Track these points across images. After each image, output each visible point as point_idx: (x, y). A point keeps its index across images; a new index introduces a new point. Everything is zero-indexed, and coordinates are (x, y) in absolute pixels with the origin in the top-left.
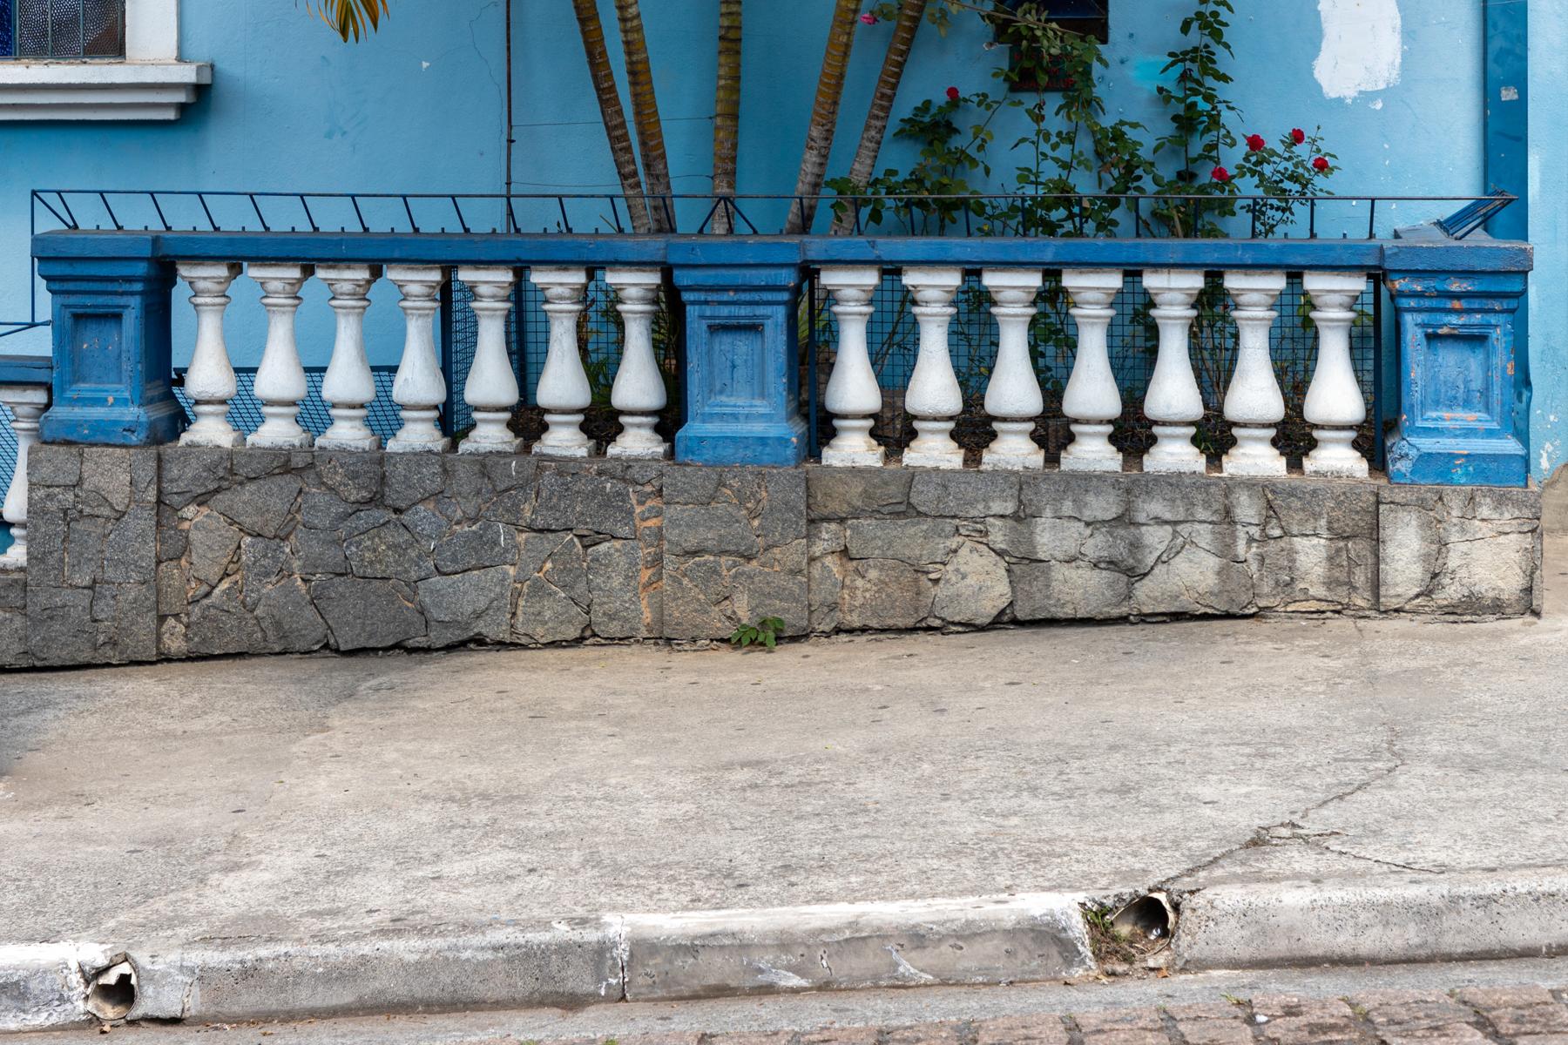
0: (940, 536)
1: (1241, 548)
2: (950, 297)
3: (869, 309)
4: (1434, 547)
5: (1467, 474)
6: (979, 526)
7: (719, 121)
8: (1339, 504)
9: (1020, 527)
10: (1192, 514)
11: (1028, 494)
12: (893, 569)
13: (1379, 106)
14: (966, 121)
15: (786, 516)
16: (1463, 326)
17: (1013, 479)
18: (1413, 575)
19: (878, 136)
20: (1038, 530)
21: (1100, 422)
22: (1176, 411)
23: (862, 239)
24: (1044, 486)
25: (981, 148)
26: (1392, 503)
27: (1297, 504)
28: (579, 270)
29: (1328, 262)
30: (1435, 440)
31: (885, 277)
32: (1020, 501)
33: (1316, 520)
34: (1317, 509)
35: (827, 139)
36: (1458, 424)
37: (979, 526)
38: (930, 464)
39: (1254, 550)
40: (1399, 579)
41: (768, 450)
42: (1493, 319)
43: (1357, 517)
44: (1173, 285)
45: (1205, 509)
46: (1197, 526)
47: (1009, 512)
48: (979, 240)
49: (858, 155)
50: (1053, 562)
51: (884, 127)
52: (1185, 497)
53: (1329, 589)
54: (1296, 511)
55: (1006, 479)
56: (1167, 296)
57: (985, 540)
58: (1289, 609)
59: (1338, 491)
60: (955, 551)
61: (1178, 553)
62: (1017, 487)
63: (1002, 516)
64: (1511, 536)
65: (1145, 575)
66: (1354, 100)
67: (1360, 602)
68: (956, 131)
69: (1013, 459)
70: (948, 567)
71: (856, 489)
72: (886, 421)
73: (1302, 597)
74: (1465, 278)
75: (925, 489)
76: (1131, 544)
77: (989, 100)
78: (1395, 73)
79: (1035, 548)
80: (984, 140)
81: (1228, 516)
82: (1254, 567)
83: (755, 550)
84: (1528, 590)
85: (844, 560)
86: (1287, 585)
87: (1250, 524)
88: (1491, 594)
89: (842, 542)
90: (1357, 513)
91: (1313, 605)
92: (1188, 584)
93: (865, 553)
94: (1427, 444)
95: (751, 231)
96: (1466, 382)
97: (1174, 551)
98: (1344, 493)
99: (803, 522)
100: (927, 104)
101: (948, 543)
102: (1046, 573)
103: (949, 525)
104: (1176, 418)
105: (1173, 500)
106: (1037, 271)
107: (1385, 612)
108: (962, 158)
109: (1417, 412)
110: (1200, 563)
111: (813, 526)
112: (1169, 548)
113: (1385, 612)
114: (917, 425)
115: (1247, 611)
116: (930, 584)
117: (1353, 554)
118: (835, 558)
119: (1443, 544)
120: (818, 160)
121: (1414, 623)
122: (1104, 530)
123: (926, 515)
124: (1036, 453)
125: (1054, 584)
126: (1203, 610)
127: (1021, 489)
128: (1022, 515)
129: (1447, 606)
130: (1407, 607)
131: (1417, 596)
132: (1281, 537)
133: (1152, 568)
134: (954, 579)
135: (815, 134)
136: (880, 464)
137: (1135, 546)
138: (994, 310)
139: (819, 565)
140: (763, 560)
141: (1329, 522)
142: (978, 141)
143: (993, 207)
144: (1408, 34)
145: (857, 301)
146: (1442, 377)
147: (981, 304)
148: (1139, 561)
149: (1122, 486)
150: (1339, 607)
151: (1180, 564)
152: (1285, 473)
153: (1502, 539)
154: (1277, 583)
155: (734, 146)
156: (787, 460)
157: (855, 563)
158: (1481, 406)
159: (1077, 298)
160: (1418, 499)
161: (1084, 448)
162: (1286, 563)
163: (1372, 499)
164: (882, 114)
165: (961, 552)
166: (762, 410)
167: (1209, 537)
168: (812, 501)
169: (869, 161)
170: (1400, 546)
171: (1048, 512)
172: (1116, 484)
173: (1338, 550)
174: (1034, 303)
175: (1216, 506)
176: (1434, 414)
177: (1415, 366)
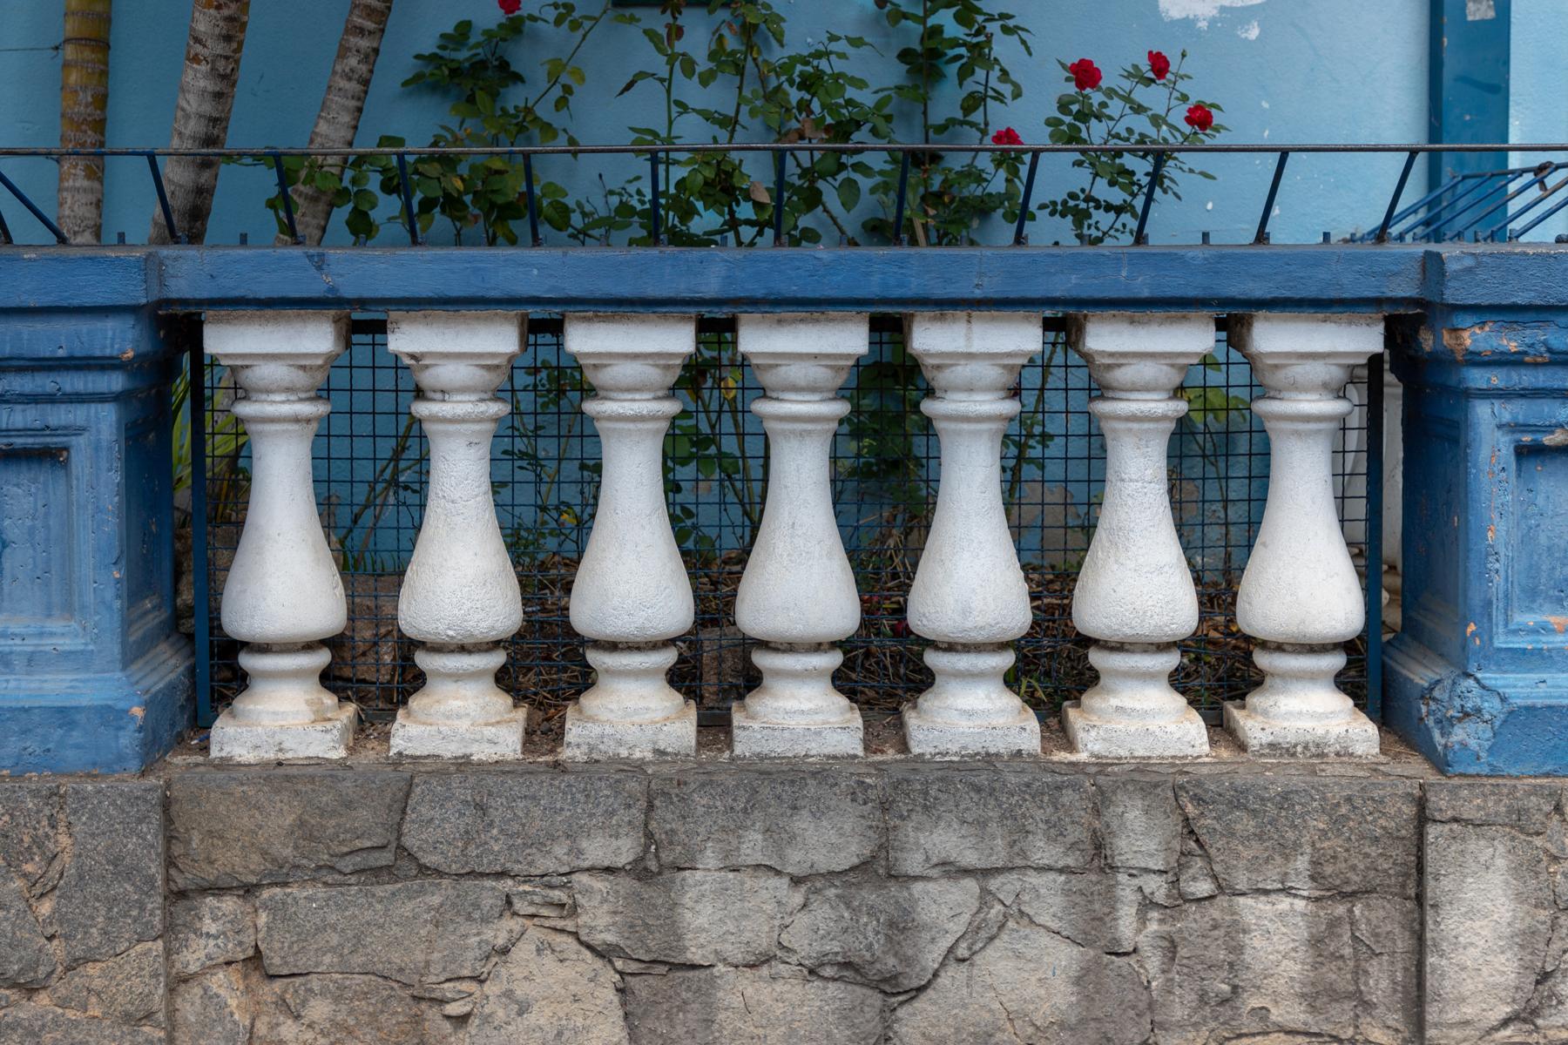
0: (469, 918)
1: (1126, 925)
2: (498, 379)
3: (321, 409)
4: (1544, 915)
6: (557, 895)
7: (70, 52)
8: (1338, 822)
9: (647, 892)
10: (1023, 854)
11: (666, 819)
12: (366, 995)
13: (1254, 33)
14: (528, 59)
15: (117, 889)
17: (632, 786)
18: (1498, 979)
19: (364, 68)
20: (687, 900)
21: (817, 647)
22: (980, 621)
23: (297, 251)
24: (700, 801)
25: (562, 103)
26: (1455, 820)
27: (1246, 824)
29: (1311, 292)
30: (1536, 676)
31: (356, 338)
32: (649, 835)
33: (1287, 858)
34: (1291, 835)
35: (228, 38)
37: (557, 895)
38: (450, 750)
39: (1153, 927)
40: (1469, 987)
41: (76, 736)
43: (1373, 851)
44: (977, 346)
45: (1051, 840)
46: (1034, 879)
47: (623, 859)
48: (558, 252)
49: (324, 106)
50: (721, 968)
51: (376, 51)
52: (1008, 815)
53: (1313, 1009)
54: (1246, 839)
55: (616, 787)
56: (963, 372)
57: (569, 925)
59: (1336, 794)
60: (505, 951)
61: (992, 939)
62: (643, 804)
63: (609, 870)
65: (921, 989)
66: (1212, 22)
68: (518, 78)
69: (631, 734)
70: (489, 988)
71: (282, 816)
72: (362, 647)
73: (1255, 1026)
75: (437, 813)
76: (892, 924)
77: (576, 15)
79: (680, 938)
80: (568, 89)
82: (1153, 963)
83: (42, 971)
85: (255, 978)
86: (1224, 1002)
87: (1147, 870)
89: (248, 939)
90: (1377, 839)
92: (1013, 1007)
93: (302, 963)
94: (1523, 686)
95: (53, 239)
97: (981, 934)
98: (1349, 799)
99: (155, 902)
100: (464, 28)
101: (488, 934)
102: (706, 993)
103: (489, 893)
104: (980, 637)
105: (982, 824)
106: (684, 319)
108: (524, 123)
109: (1499, 617)
110: (1039, 960)
111: (182, 904)
112: (974, 929)
114: (423, 660)
116: (447, 1027)
117: (1363, 931)
118: (234, 974)
120: (211, 86)
122: (832, 892)
123: (439, 873)
124: (681, 716)
125: (721, 1016)
127: (651, 807)
128: (652, 865)
131: (1505, 1023)
132: (1211, 897)
133: (936, 975)
134: (501, 1013)
135: (202, 27)
136: (340, 753)
137: (900, 926)
138: (590, 407)
139: (198, 991)
140: (62, 991)
141: (1315, 863)
142: (557, 92)
143: (584, 214)
145: (288, 390)
146: (1543, 540)
147: (561, 392)
148: (908, 961)
149: (872, 794)
151: (997, 963)
152: (1206, 748)
154: (1203, 998)
155: (102, 100)
156: (121, 758)
157: (278, 985)
159: (768, 379)
160: (1510, 811)
161: (781, 704)
162: (1222, 955)
163: (1409, 810)
164: (370, 25)
165: (516, 954)
166: (66, 644)
167: (1058, 902)
168: (177, 849)
169: (346, 118)
170: (1471, 914)
171: (710, 858)
172: (858, 792)
173: (1334, 923)
174: (672, 392)
175: (1074, 834)
176: (1530, 619)
177: (1495, 515)
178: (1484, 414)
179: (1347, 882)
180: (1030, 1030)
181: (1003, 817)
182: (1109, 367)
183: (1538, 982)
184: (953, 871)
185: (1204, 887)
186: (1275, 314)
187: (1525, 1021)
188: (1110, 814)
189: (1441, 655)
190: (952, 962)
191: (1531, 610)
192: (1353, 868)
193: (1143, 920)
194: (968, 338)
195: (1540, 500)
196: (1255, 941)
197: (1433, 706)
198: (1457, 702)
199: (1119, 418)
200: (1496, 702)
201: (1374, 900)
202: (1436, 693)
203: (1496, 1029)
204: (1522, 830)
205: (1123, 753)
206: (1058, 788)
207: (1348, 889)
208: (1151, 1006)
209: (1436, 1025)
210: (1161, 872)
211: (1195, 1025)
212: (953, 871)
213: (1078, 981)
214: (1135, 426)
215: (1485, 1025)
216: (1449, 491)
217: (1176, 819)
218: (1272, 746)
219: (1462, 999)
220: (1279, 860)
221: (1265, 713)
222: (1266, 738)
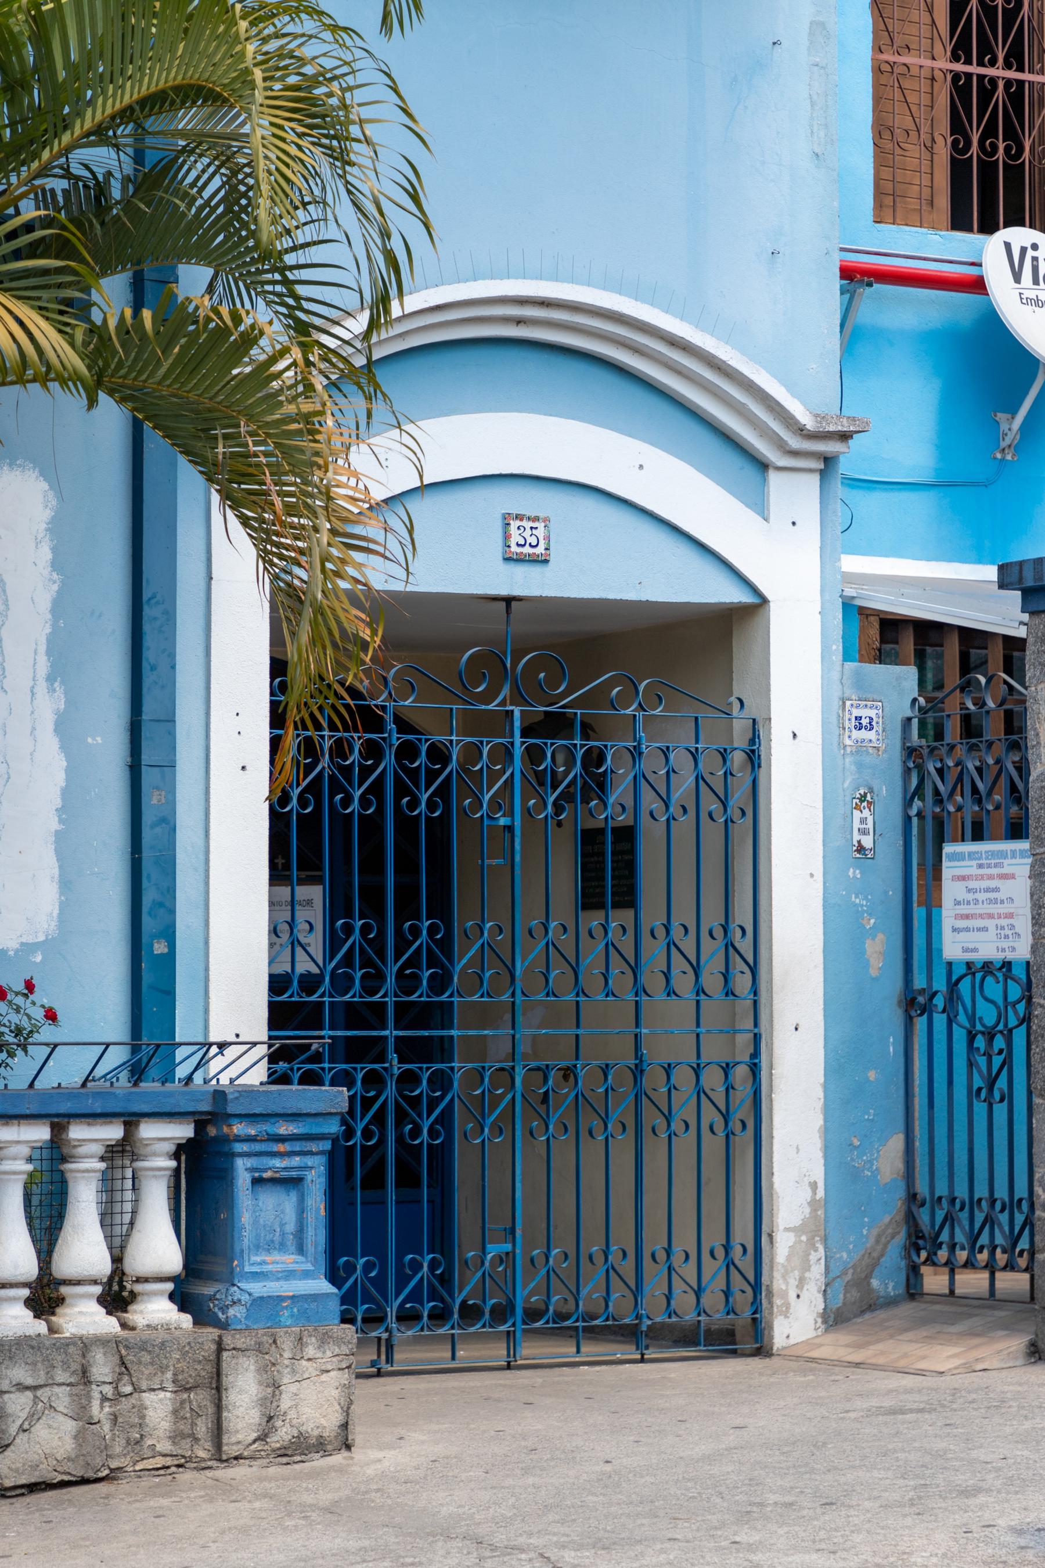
4: (270, 1390)
5: (292, 1316)
13: (39, 958)
16: (285, 1169)
26: (234, 1349)
27: (146, 1358)
28: (44, 1123)
30: (262, 1284)
33: (163, 1373)
34: (165, 1362)
36: (279, 1267)
39: (107, 1409)
40: (240, 1426)
42: (309, 1161)
43: (199, 1367)
45: (64, 1370)
46: (57, 1390)
52: (46, 1359)
58: (137, 1468)
59: (184, 1341)
61: (39, 1419)
64: (332, 1373)
65: (8, 1446)
66: (17, 951)
67: (202, 1454)
74: (292, 1121)
78: (53, 924)
81: (84, 1377)
82: (107, 1427)
84: (345, 1426)
87: (104, 1383)
88: (316, 1433)
90: (200, 1362)
91: (159, 1462)
92: (47, 1451)
94: (258, 1288)
96: (282, 1225)
97: (33, 1417)
98: (189, 1343)
105: (34, 1364)
107: (226, 1461)
110: (58, 1428)
113: (226, 1461)
115: (101, 1475)
117: (195, 1405)
119: (277, 1386)
121: (254, 1469)
126: (60, 1478)
129: (279, 1449)
130: (246, 1454)
131: (254, 1441)
132: (131, 1394)
141: (175, 1375)
144: (66, 884)
146: (261, 1221)
150: (183, 1461)
151: (40, 1431)
153: (324, 1377)
154: (128, 1442)
158: (293, 1248)
162: (137, 1420)
163: (214, 1347)
167: (66, 1400)
170: (240, 1392)
173: (182, 1402)
176: (258, 1259)
178: (240, 1163)
179: (188, 1383)
180: (55, 1462)
181: (43, 1360)
182: (75, 1147)
183: (268, 1422)
184: (22, 1387)
185: (128, 1389)
186: (151, 1120)
187: (262, 1440)
188: (89, 1355)
189: (216, 1280)
190: (21, 1432)
191: (257, 1255)
192: (190, 1376)
193: (102, 1407)
194: (19, 1134)
195: (260, 1204)
196: (150, 1413)
197: (216, 1302)
198: (230, 1298)
199: (79, 1171)
200: (247, 1296)
201: (199, 1391)
202: (218, 1296)
203: (250, 1445)
204: (260, 1352)
205: (84, 1332)
206: (67, 1345)
207: (188, 1386)
208: (106, 1447)
209: (227, 1444)
210: (110, 1383)
211: (125, 1455)
212: (22, 1387)
213: (75, 1437)
214: (86, 1175)
215: (247, 1443)
216: (217, 1203)
217: (117, 1357)
218: (148, 1326)
219: (237, 1432)
220: (160, 1374)
221: (141, 1312)
222: (145, 1322)
